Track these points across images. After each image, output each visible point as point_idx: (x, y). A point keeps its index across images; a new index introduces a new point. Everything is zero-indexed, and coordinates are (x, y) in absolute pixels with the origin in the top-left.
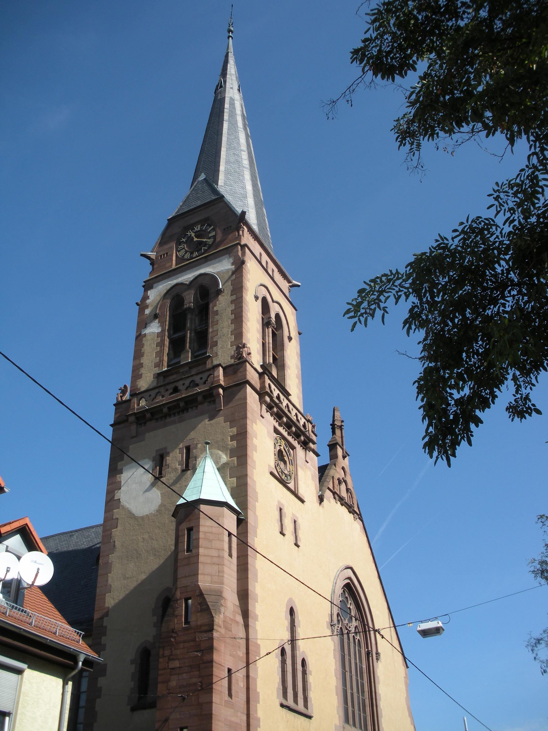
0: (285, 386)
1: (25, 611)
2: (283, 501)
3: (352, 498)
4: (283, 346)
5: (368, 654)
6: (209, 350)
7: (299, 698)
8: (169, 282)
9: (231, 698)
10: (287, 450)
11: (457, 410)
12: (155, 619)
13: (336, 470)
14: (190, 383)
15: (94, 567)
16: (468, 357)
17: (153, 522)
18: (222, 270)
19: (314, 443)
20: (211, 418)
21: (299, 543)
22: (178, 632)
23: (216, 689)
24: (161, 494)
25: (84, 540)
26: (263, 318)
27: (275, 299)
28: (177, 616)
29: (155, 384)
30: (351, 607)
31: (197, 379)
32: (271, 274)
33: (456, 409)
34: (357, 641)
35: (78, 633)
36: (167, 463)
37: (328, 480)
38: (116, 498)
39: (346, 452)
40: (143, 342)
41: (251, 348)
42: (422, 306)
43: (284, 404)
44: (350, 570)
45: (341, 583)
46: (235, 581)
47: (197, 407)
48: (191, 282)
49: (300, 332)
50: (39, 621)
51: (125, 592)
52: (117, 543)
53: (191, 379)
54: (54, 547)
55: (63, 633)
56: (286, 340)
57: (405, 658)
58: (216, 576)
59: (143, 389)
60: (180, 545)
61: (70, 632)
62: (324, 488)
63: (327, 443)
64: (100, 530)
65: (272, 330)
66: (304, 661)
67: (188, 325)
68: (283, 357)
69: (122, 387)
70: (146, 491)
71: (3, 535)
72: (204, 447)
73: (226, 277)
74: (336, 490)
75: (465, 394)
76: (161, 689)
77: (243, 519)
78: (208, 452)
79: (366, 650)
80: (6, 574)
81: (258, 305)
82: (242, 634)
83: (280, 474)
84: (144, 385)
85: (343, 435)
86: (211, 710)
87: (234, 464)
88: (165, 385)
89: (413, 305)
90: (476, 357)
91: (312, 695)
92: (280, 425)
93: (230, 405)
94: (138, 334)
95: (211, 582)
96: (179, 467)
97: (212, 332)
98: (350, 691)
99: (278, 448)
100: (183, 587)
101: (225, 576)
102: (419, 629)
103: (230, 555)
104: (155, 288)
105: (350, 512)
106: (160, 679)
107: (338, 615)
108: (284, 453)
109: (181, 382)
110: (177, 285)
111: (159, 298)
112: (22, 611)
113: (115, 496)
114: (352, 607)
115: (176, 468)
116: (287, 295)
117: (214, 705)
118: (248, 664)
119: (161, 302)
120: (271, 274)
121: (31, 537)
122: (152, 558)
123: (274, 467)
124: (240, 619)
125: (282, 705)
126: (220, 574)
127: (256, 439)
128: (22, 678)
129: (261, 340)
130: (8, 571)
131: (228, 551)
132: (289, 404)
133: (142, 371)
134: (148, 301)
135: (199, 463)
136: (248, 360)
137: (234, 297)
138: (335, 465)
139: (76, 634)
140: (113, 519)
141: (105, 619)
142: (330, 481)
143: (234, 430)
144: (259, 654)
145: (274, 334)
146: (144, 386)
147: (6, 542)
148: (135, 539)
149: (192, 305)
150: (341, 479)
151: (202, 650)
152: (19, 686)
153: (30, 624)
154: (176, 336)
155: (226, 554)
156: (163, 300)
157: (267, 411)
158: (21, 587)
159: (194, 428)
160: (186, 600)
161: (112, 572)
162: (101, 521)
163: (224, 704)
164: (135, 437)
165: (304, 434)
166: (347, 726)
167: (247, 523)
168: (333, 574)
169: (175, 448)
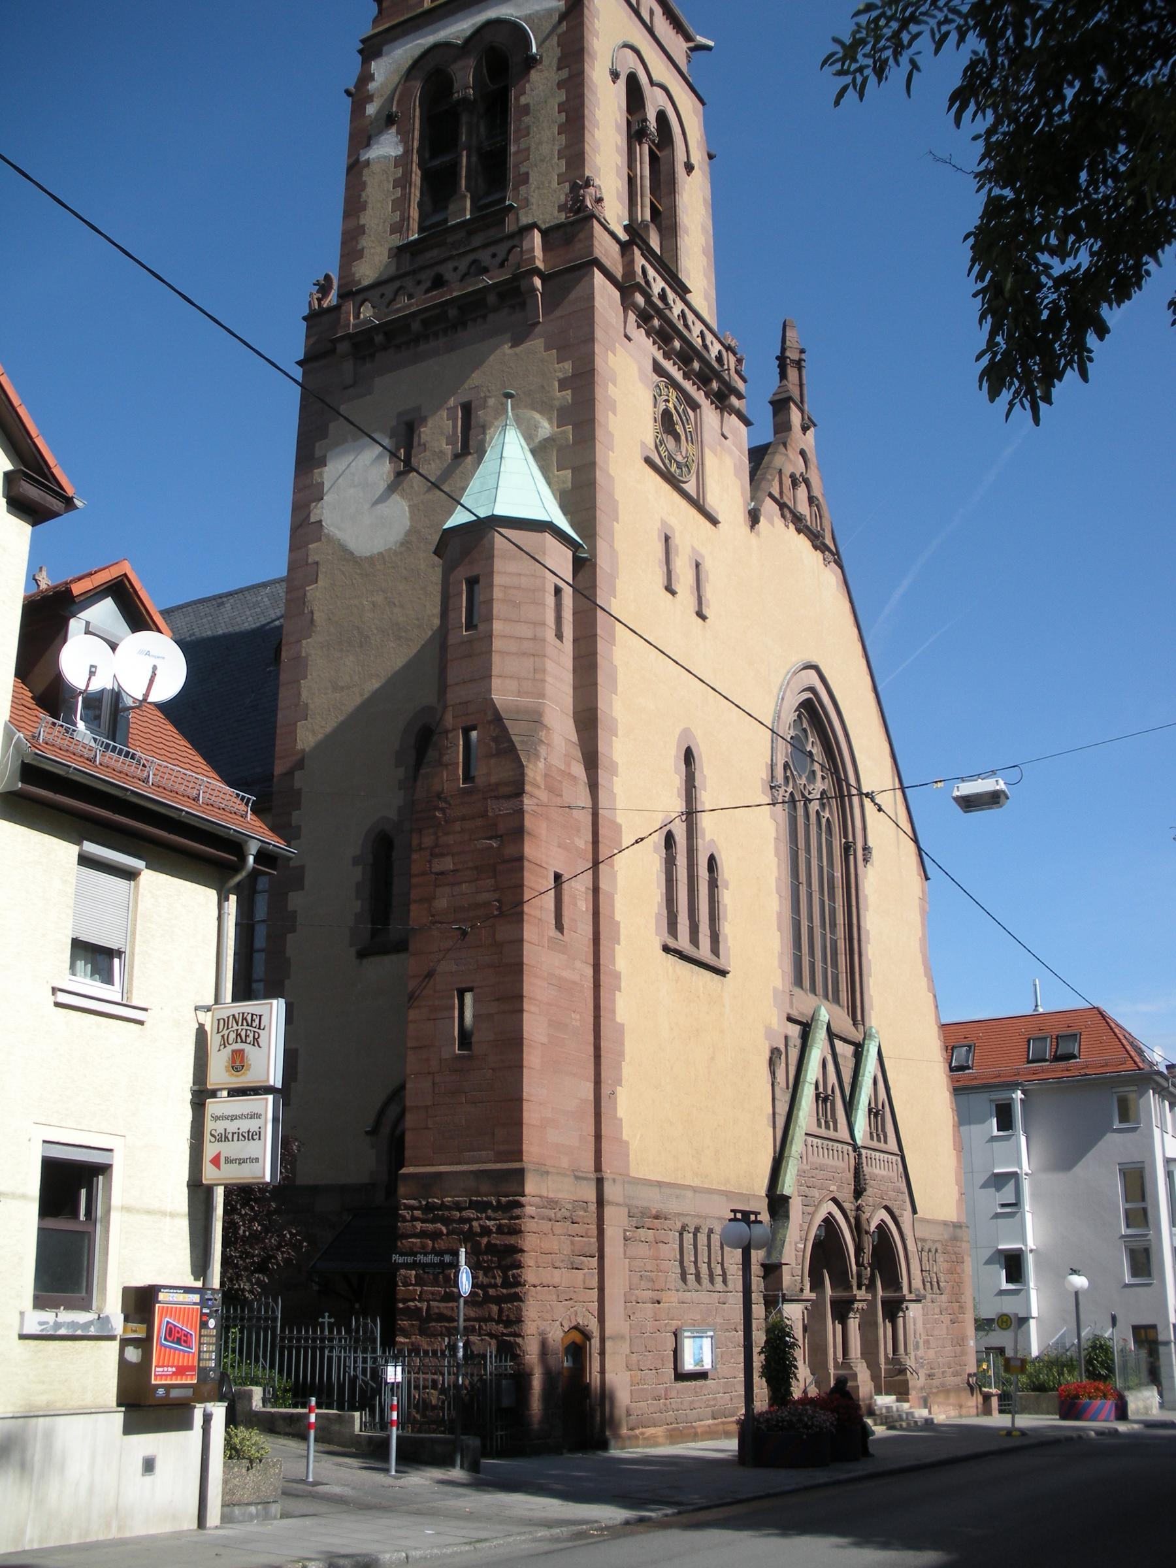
0: (677, 270)
1: (134, 754)
2: (673, 521)
3: (820, 517)
4: (674, 183)
5: (847, 849)
6: (509, 194)
7: (701, 935)
8: (419, 41)
9: (562, 933)
10: (681, 411)
11: (1059, 299)
12: (400, 773)
13: (787, 455)
14: (470, 267)
15: (272, 669)
16: (1092, 182)
17: (394, 568)
18: (537, 12)
19: (740, 396)
20: (517, 342)
21: (706, 612)
22: (449, 799)
23: (530, 915)
24: (410, 506)
25: (248, 613)
26: (629, 123)
27: (655, 77)
28: (446, 765)
29: (392, 271)
30: (814, 751)
31: (485, 257)
32: (648, 21)
33: (1055, 296)
34: (824, 821)
35: (243, 799)
36: (422, 441)
37: (770, 477)
38: (312, 520)
39: (809, 418)
40: (364, 179)
41: (602, 187)
42: (994, 62)
43: (676, 311)
44: (812, 672)
45: (794, 699)
46: (570, 691)
47: (484, 317)
48: (468, 40)
49: (713, 152)
50: (163, 775)
51: (337, 717)
52: (317, 616)
53: (471, 257)
54: (186, 630)
55: (213, 798)
56: (680, 170)
57: (919, 849)
58: (528, 679)
59: (366, 283)
60: (452, 615)
61: (227, 797)
62: (760, 494)
63: (769, 397)
64: (281, 590)
65: (650, 149)
66: (712, 861)
67: (464, 139)
68: (673, 208)
69: (321, 279)
70: (376, 503)
71: (77, 600)
72: (502, 404)
73: (547, 27)
74: (785, 499)
75: (1079, 266)
76: (417, 915)
77: (586, 559)
78: (510, 414)
79: (843, 840)
80: (89, 679)
81: (620, 89)
82: (584, 799)
83: (667, 461)
84: (368, 273)
85: (804, 381)
86: (522, 956)
87: (567, 439)
88: (414, 272)
89: (974, 58)
90: (1110, 182)
91: (727, 929)
92: (667, 356)
93: (558, 313)
94: (352, 160)
95: (519, 694)
96: (448, 449)
97: (516, 153)
98: (806, 923)
99: (662, 406)
100: (460, 704)
101: (549, 679)
102: (956, 793)
103: (559, 636)
104: (388, 54)
105: (816, 548)
106: (414, 895)
107: (786, 766)
108: (676, 417)
109: (451, 265)
110: (436, 46)
111: (396, 79)
112: (127, 754)
113: (312, 515)
114: (817, 750)
115: (441, 452)
116: (684, 69)
117: (526, 945)
118: (596, 863)
119: (400, 86)
120: (647, 18)
121: (138, 607)
122: (392, 645)
123: (652, 446)
124: (579, 770)
125: (666, 949)
126: (537, 676)
127: (615, 385)
128: (137, 887)
129: (625, 170)
130: (92, 673)
131: (554, 627)
132: (687, 310)
133: (364, 242)
134: (372, 86)
135: (492, 439)
136: (597, 213)
137: (564, 74)
138: (785, 445)
139: (238, 801)
140: (307, 564)
141: (298, 774)
142: (773, 480)
143: (568, 366)
144: (620, 843)
145: (653, 158)
146: (368, 276)
147: (86, 615)
148: (355, 606)
149: (472, 91)
150: (798, 476)
151: (501, 836)
152: (131, 907)
153: (145, 780)
154: (436, 162)
155: (550, 634)
156: (405, 81)
157: (639, 327)
158: (121, 706)
159: (478, 363)
160: (466, 731)
161: (309, 677)
162: (284, 573)
163: (546, 945)
164: (351, 386)
165: (718, 376)
166: (798, 991)
167: (594, 566)
168: (777, 679)
169: (439, 408)
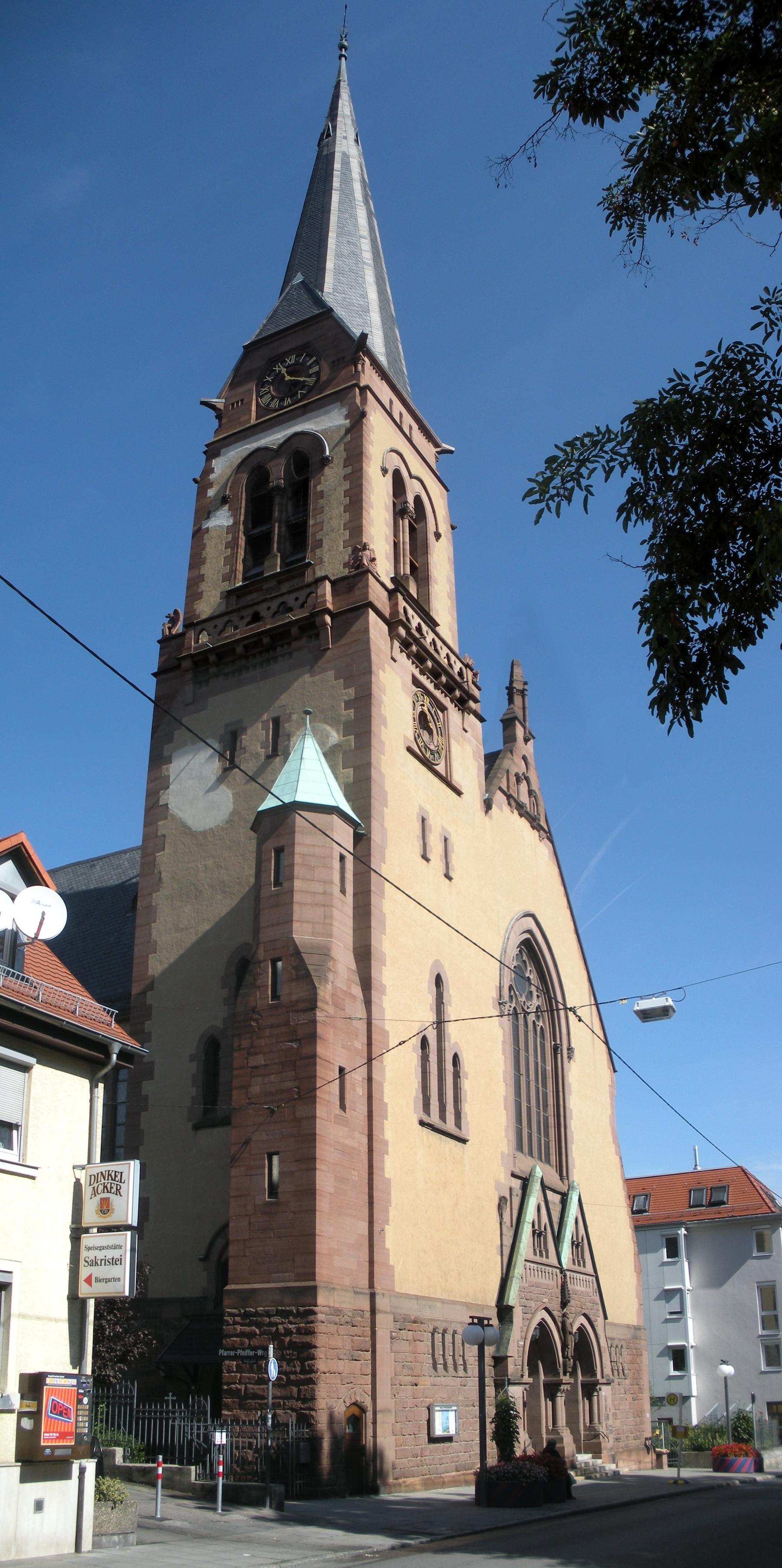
66: (456, 1059)
